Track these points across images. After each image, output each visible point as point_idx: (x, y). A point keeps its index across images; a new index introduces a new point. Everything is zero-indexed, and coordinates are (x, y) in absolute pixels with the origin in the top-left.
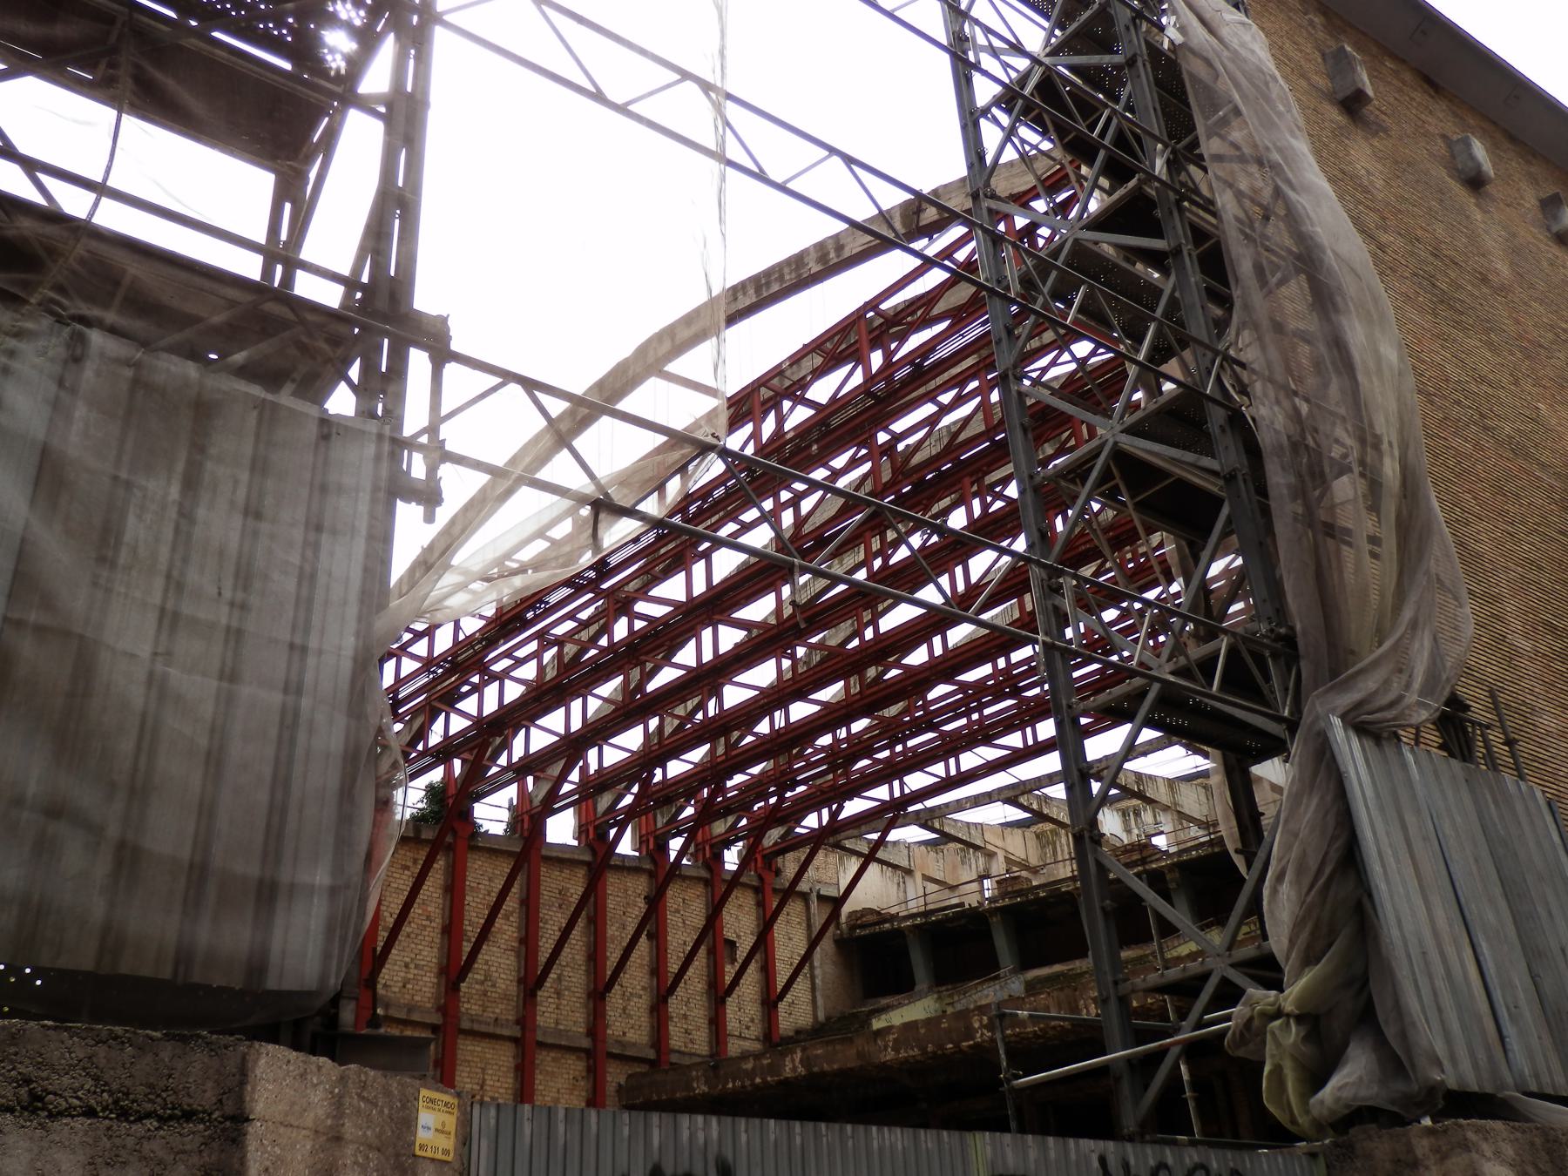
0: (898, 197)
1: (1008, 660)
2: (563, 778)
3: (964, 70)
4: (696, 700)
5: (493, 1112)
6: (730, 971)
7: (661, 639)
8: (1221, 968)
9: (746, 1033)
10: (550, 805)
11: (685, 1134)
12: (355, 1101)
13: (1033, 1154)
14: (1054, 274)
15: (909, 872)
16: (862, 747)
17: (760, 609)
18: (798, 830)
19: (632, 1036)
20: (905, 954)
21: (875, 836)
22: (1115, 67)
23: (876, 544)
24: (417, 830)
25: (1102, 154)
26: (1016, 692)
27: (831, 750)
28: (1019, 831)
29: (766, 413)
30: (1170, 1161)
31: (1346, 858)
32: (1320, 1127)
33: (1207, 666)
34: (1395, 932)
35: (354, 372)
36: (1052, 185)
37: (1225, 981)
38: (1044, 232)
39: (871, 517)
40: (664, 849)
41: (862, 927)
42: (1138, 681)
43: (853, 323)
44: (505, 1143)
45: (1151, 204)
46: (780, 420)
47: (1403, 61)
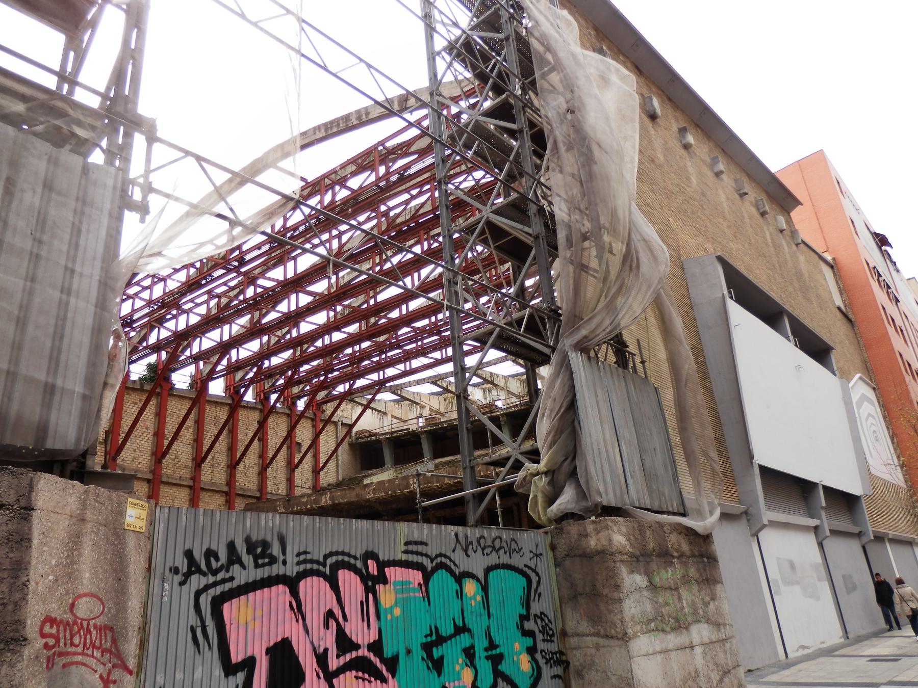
0: (398, 92)
2: (218, 362)
3: (430, 30)
4: (287, 329)
5: (167, 510)
6: (298, 457)
7: (271, 298)
8: (516, 455)
9: (304, 485)
10: (211, 376)
11: (263, 522)
12: (93, 503)
13: (426, 532)
14: (466, 135)
15: (385, 414)
16: (366, 355)
17: (320, 287)
18: (334, 393)
19: (248, 486)
20: (381, 450)
21: (370, 397)
22: (501, 40)
23: (377, 260)
24: (142, 385)
25: (491, 80)
26: (439, 333)
27: (352, 356)
29: (327, 191)
30: (486, 535)
31: (571, 406)
32: (550, 521)
33: (519, 322)
34: (588, 440)
35: (104, 143)
36: (469, 94)
37: (517, 461)
38: (464, 117)
39: (375, 246)
40: (267, 399)
41: (362, 438)
42: (490, 327)
43: (372, 151)
44: (173, 525)
45: (511, 107)
46: (334, 195)
47: (627, 57)
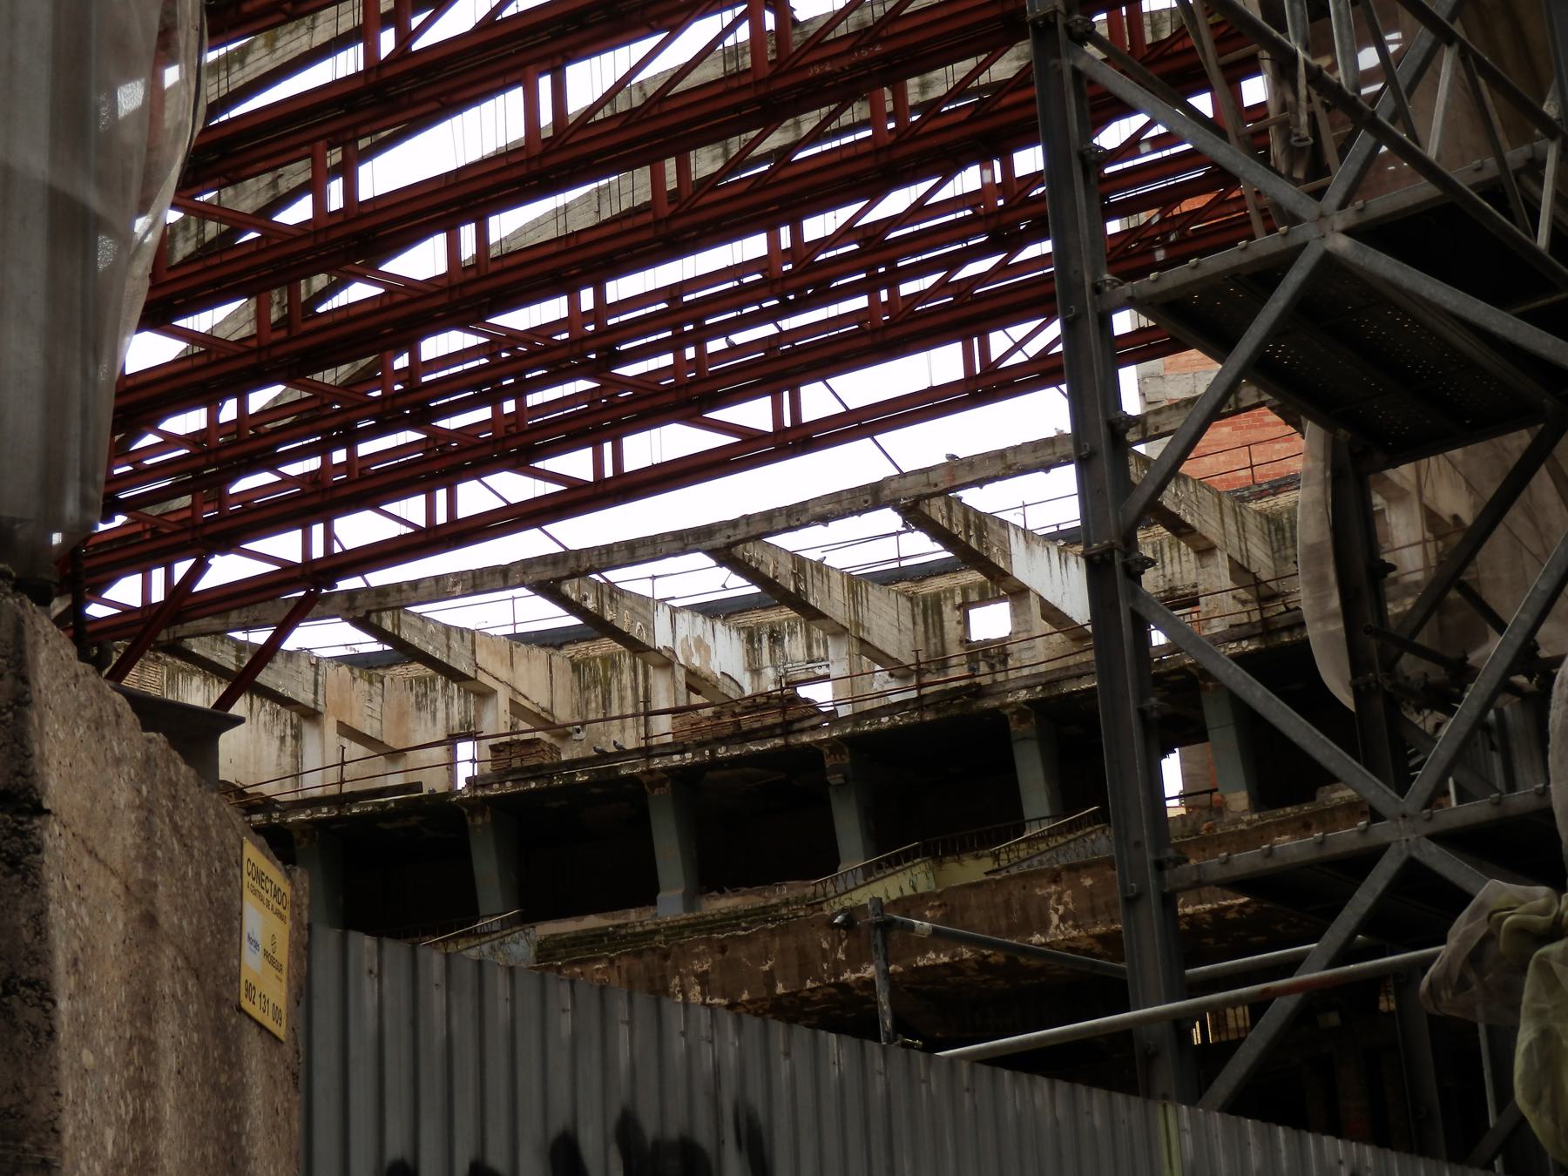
1: (600, 295)
8: (1404, 836)
15: (311, 715)
16: (253, 445)
18: (96, 610)
21: (260, 637)
28: (543, 654)
37: (1413, 875)
